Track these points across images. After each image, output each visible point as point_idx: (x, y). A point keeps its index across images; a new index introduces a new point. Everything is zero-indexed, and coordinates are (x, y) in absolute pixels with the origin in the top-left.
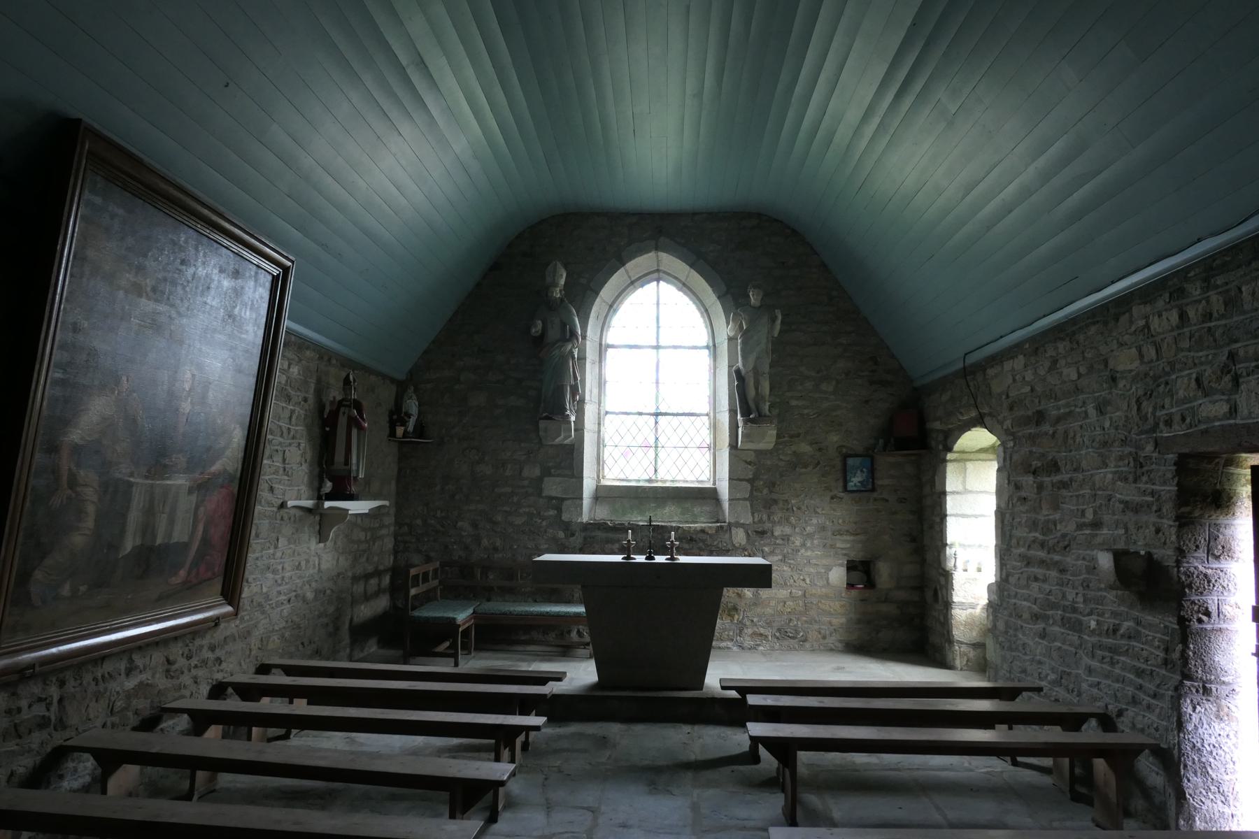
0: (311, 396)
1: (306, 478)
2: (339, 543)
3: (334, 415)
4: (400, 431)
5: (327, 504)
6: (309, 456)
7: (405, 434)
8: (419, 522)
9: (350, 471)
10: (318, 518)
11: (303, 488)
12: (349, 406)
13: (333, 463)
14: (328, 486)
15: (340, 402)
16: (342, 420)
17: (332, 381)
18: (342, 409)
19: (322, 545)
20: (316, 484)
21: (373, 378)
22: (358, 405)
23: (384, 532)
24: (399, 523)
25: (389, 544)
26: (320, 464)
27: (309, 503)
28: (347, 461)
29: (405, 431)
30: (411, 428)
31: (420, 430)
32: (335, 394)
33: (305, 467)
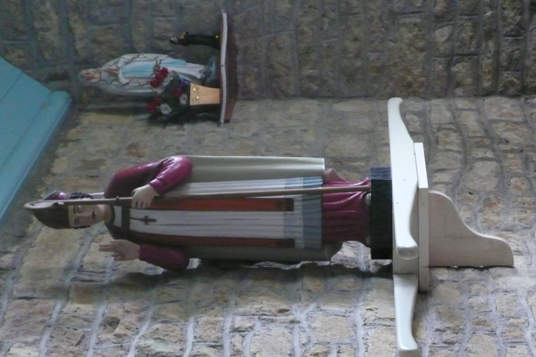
0: (103, 309)
1: (334, 308)
2: (509, 220)
3: (154, 246)
4: (201, 96)
5: (403, 238)
6: (267, 304)
7: (210, 81)
8: (441, 34)
9: (308, 194)
10: (443, 274)
11: (360, 313)
12: (126, 207)
13: (289, 243)
14: (354, 252)
15: (116, 233)
16: (168, 223)
17: (61, 261)
18: (136, 226)
19: (518, 261)
20: (348, 282)
21: (60, 166)
22: (123, 185)
23: (470, 120)
24: (448, 87)
25: (500, 108)
26: (293, 276)
27: (403, 296)
28: (283, 204)
29: (203, 82)
30: (195, 70)
31: (198, 43)
32: (93, 250)
33: (300, 312)
